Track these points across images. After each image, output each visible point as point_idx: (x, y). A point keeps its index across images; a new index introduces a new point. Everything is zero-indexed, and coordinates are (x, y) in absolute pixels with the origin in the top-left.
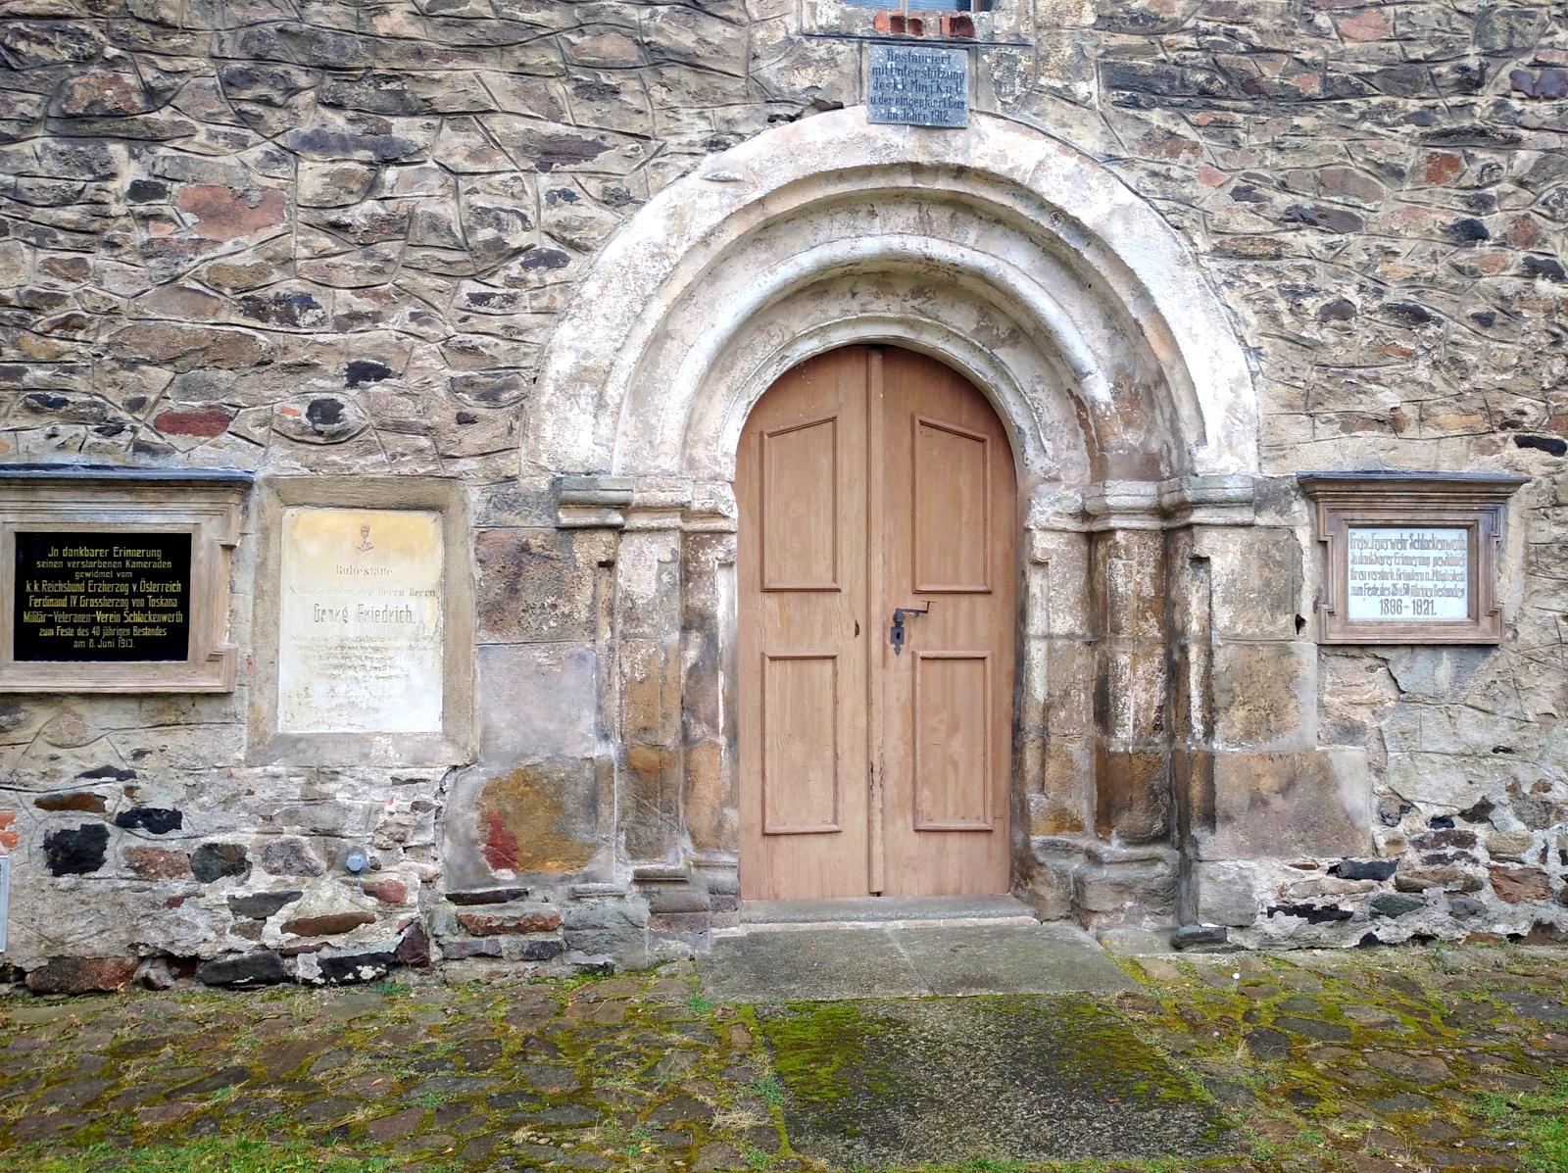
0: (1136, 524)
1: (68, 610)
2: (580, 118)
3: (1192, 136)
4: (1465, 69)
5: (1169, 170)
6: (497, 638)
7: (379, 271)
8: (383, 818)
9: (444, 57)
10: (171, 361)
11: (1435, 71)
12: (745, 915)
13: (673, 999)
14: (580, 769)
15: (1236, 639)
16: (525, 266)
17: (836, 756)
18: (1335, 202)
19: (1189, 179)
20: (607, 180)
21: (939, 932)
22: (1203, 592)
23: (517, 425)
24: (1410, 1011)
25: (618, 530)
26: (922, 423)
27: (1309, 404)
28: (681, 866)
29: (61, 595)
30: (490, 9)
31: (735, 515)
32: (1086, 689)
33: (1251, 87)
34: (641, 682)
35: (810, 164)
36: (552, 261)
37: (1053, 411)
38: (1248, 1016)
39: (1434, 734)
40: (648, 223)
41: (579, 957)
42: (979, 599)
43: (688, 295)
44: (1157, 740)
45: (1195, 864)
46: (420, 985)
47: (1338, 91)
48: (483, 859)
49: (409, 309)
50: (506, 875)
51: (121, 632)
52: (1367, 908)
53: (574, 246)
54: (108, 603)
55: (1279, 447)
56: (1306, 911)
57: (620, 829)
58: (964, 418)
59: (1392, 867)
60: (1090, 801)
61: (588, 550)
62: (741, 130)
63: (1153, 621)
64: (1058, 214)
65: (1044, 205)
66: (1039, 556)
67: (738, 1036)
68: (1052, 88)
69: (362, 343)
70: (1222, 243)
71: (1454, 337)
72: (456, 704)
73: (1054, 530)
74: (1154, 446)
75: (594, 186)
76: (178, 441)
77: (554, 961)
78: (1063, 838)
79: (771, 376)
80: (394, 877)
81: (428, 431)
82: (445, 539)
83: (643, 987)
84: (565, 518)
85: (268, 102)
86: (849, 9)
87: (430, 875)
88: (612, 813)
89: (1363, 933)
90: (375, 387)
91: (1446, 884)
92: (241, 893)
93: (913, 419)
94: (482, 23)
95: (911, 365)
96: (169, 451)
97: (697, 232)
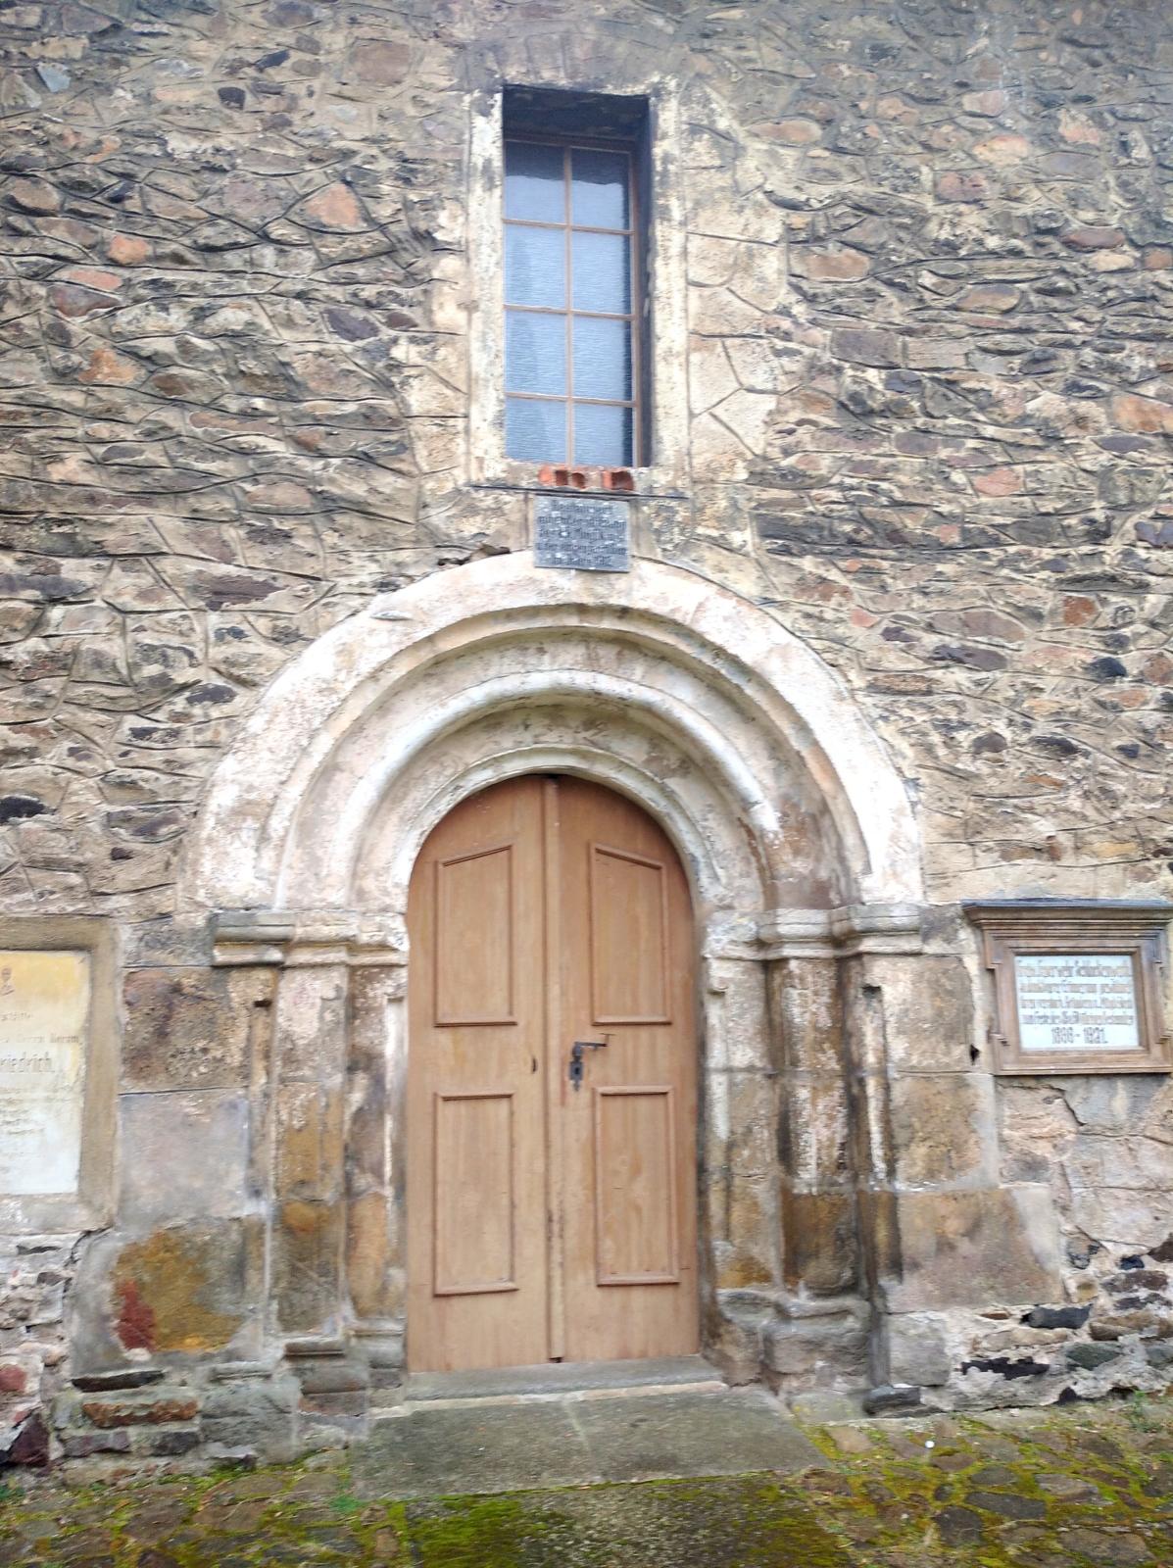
0: (808, 952)
2: (250, 561)
3: (843, 581)
4: (1092, 521)
6: (141, 1087)
7: (39, 707)
9: (118, 502)
11: (1066, 522)
12: (410, 1391)
13: (317, 1500)
14: (226, 1232)
15: (912, 1071)
16: (190, 701)
17: (513, 1206)
18: (981, 642)
19: (841, 621)
21: (620, 1403)
22: (878, 1022)
23: (175, 860)
24: (1107, 1478)
25: (278, 967)
26: (599, 851)
27: (968, 833)
28: (337, 1338)
31: (405, 947)
33: (896, 537)
34: (300, 1130)
35: (479, 604)
36: (218, 696)
37: (724, 839)
38: (939, 1494)
39: (1116, 1169)
40: (317, 660)
41: (217, 1450)
42: (660, 1031)
43: (358, 728)
44: (841, 1180)
45: (885, 1317)
46: (38, 1488)
47: (977, 541)
48: (115, 1337)
49: (68, 744)
50: (140, 1355)
52: (1064, 1360)
53: (241, 681)
55: (941, 875)
56: (999, 1366)
57: (272, 1297)
58: (640, 846)
59: (1084, 1313)
61: (244, 989)
62: (411, 572)
63: (831, 1053)
64: (719, 652)
65: (705, 644)
66: (716, 985)
67: (383, 1544)
71: (1102, 768)
72: (94, 1161)
73: (729, 959)
75: (263, 624)
77: (190, 1456)
78: (750, 1290)
79: (445, 805)
80: (13, 1362)
81: (79, 868)
82: (93, 980)
83: (286, 1483)
84: (220, 956)
86: (515, 464)
87: (53, 1359)
88: (264, 1278)
89: (1061, 1387)
90: (27, 824)
91: (1140, 1329)
93: (588, 846)
94: (158, 472)
95: (583, 795)
97: (365, 667)
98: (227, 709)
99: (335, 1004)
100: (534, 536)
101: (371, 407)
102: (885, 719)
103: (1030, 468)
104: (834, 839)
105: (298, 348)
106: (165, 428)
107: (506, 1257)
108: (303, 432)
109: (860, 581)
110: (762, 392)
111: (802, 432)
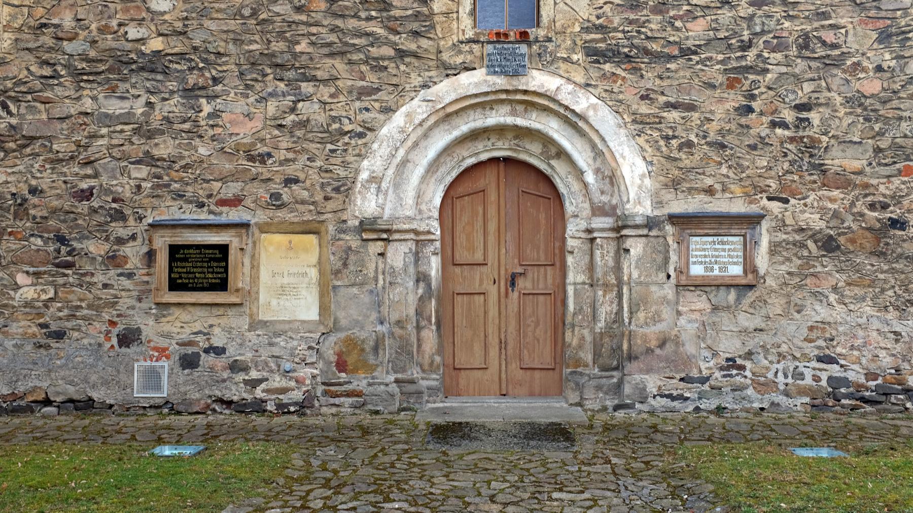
0: (605, 235)
1: (187, 273)
2: (372, 78)
3: (623, 74)
4: (742, 41)
8: (297, 352)
10: (221, 180)
15: (641, 283)
16: (350, 138)
17: (486, 336)
19: (621, 92)
27: (674, 185)
29: (184, 267)
31: (438, 233)
35: (462, 92)
36: (361, 135)
37: (576, 186)
40: (399, 118)
43: (416, 144)
49: (307, 156)
50: (343, 375)
51: (205, 281)
54: (200, 270)
55: (661, 203)
56: (670, 397)
58: (543, 189)
62: (435, 80)
63: (613, 276)
64: (567, 108)
65: (561, 105)
66: (569, 249)
69: (291, 170)
74: (614, 202)
76: (225, 209)
79: (454, 174)
81: (313, 203)
85: (256, 80)
90: (294, 187)
92: (247, 378)
96: (221, 214)
97: (417, 122)
98: (364, 140)
99: (410, 255)
101: (418, 12)
102: (639, 136)
103: (713, 17)
106: (338, 27)
108: (391, 24)
109: (631, 74)
111: (607, 8)
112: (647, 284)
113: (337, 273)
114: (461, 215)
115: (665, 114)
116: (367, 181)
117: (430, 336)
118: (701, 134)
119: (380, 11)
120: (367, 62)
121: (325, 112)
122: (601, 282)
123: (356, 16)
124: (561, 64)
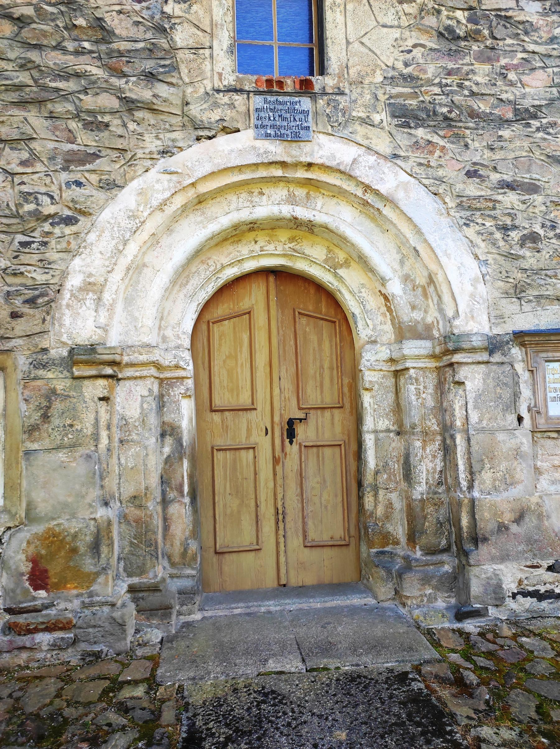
2: (86, 140)
3: (442, 143)
5: (429, 161)
15: (483, 430)
17: (257, 506)
19: (441, 166)
20: (102, 175)
27: (518, 292)
30: (32, 81)
31: (191, 367)
32: (398, 461)
35: (223, 163)
36: (69, 221)
40: (127, 198)
44: (440, 491)
45: (467, 567)
48: (27, 584)
50: (42, 593)
55: (501, 317)
56: (535, 594)
60: (403, 525)
62: (180, 144)
63: (434, 421)
64: (367, 188)
66: (367, 386)
68: (359, 117)
70: (462, 202)
75: (94, 178)
79: (211, 289)
82: (5, 387)
94: (28, 89)
97: (155, 203)
98: (74, 228)
100: (253, 121)
102: (467, 225)
104: (436, 299)
105: (107, 8)
106: (31, 61)
107: (254, 533)
109: (453, 143)
110: (391, 27)
111: (417, 53)
112: (492, 432)
113: (31, 430)
114: (220, 345)
115: (500, 198)
116: (81, 289)
117: (181, 512)
118: (549, 224)
119: (97, 42)
120: (78, 116)
121: (13, 187)
122: (418, 429)
123: (59, 47)
124: (357, 127)
